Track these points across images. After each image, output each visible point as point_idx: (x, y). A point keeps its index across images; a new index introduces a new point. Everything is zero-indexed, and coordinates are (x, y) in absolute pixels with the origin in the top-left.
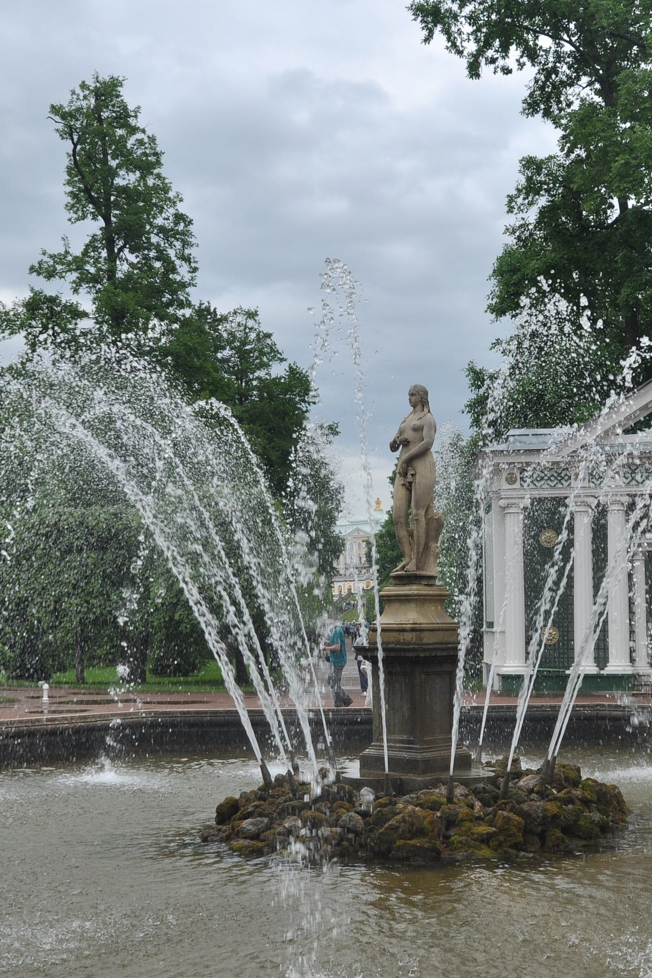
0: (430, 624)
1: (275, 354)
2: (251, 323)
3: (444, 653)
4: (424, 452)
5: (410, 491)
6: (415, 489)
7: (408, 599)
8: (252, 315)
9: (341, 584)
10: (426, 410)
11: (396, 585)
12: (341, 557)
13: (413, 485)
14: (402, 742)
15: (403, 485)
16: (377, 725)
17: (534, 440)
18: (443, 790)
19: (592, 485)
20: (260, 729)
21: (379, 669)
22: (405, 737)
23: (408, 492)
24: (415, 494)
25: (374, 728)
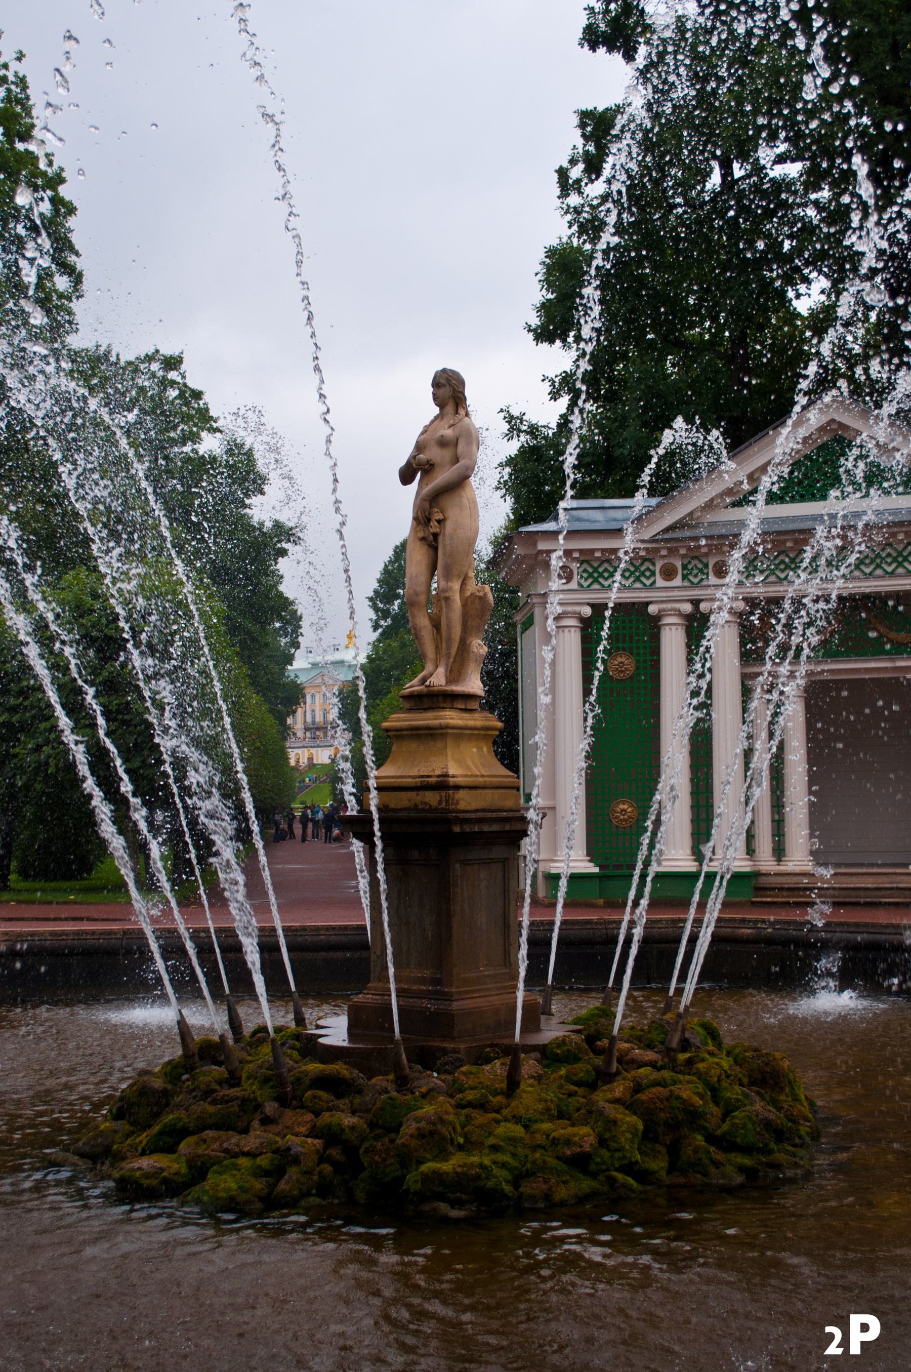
0: (471, 776)
1: (205, 419)
2: (173, 375)
3: (496, 827)
4: (459, 483)
5: (436, 549)
6: (445, 546)
7: (431, 735)
8: (172, 363)
9: (299, 751)
10: (462, 412)
11: (410, 710)
12: (300, 711)
13: (440, 539)
14: (423, 981)
15: (423, 539)
16: (379, 953)
17: (597, 515)
18: (497, 1069)
19: (686, 584)
20: (231, 956)
21: (376, 862)
22: (427, 973)
23: (431, 552)
24: (444, 554)
25: (373, 957)
